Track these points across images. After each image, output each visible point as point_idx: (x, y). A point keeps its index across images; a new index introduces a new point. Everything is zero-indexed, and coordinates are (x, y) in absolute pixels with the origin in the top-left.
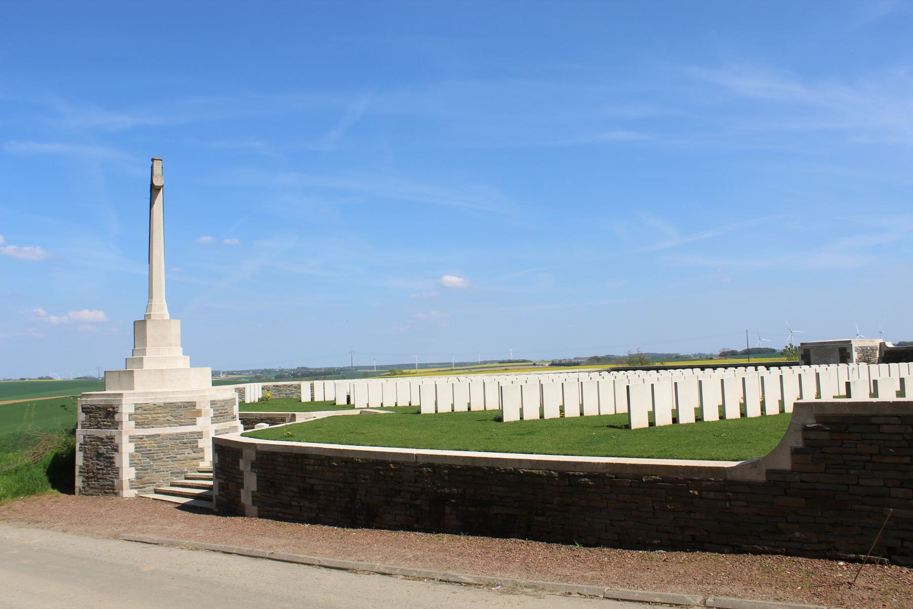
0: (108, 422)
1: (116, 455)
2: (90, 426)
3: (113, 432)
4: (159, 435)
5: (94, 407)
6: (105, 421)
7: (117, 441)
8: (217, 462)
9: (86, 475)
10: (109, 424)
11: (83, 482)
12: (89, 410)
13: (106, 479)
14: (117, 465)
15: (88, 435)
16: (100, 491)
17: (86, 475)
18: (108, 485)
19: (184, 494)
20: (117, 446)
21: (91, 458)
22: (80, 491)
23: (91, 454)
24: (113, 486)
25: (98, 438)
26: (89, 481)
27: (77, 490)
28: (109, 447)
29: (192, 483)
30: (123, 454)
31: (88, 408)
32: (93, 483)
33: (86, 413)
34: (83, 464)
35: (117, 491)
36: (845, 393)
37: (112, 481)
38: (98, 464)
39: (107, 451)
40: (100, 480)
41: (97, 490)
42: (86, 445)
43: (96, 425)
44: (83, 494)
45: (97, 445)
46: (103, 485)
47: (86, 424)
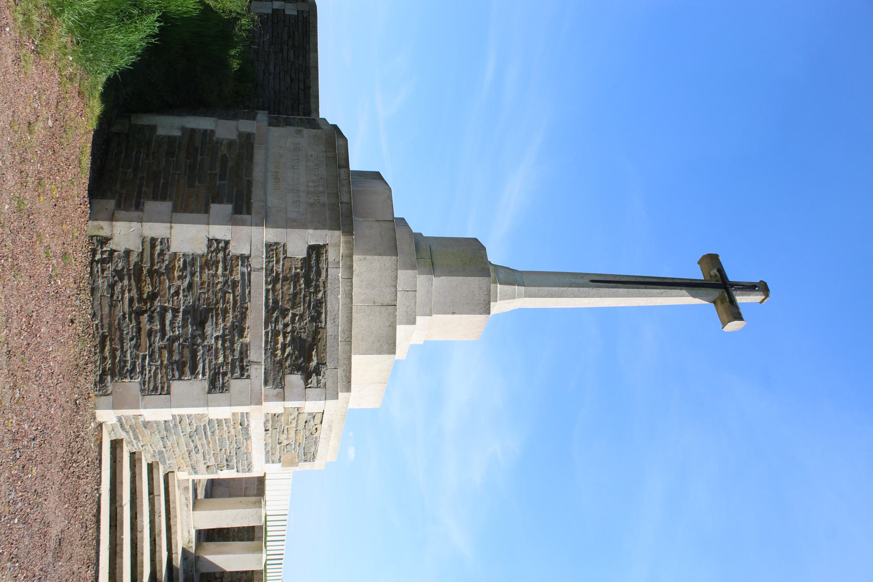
0: (284, 347)
1: (201, 384)
2: (274, 280)
3: (257, 372)
4: (248, 437)
5: (320, 295)
6: (285, 337)
7: (236, 385)
8: (166, 206)
9: (146, 266)
10: (279, 352)
11: (128, 253)
12: (313, 276)
13: (137, 347)
14: (177, 386)
15: (249, 274)
16: (106, 321)
17: (146, 266)
18: (124, 353)
19: (118, 560)
20: (224, 388)
21: (190, 286)
22: (104, 241)
23: (202, 284)
24: (123, 376)
25: (243, 316)
26: (130, 279)
27: (104, 228)
28: (221, 360)
29: (142, 531)
30: (206, 408)
31: (319, 274)
32: (126, 292)
33: (306, 261)
34: (175, 254)
35: (110, 389)
36: (268, 554)
37: (133, 370)
38: (175, 311)
39: (210, 348)
40: (134, 323)
41: (106, 310)
42: (225, 269)
43: (276, 302)
44: (94, 255)
45: (225, 311)
46: (122, 331)
47: (278, 262)
